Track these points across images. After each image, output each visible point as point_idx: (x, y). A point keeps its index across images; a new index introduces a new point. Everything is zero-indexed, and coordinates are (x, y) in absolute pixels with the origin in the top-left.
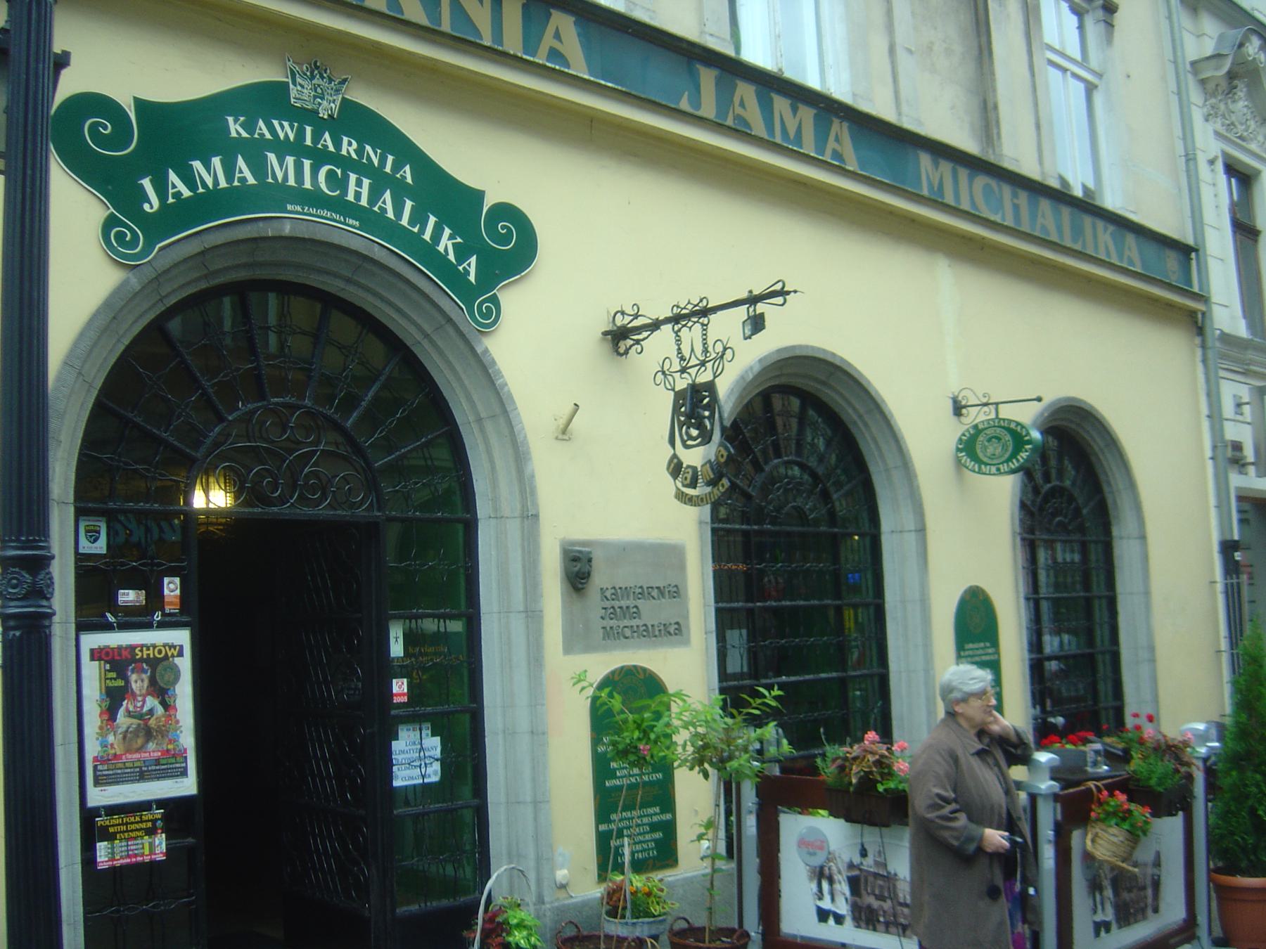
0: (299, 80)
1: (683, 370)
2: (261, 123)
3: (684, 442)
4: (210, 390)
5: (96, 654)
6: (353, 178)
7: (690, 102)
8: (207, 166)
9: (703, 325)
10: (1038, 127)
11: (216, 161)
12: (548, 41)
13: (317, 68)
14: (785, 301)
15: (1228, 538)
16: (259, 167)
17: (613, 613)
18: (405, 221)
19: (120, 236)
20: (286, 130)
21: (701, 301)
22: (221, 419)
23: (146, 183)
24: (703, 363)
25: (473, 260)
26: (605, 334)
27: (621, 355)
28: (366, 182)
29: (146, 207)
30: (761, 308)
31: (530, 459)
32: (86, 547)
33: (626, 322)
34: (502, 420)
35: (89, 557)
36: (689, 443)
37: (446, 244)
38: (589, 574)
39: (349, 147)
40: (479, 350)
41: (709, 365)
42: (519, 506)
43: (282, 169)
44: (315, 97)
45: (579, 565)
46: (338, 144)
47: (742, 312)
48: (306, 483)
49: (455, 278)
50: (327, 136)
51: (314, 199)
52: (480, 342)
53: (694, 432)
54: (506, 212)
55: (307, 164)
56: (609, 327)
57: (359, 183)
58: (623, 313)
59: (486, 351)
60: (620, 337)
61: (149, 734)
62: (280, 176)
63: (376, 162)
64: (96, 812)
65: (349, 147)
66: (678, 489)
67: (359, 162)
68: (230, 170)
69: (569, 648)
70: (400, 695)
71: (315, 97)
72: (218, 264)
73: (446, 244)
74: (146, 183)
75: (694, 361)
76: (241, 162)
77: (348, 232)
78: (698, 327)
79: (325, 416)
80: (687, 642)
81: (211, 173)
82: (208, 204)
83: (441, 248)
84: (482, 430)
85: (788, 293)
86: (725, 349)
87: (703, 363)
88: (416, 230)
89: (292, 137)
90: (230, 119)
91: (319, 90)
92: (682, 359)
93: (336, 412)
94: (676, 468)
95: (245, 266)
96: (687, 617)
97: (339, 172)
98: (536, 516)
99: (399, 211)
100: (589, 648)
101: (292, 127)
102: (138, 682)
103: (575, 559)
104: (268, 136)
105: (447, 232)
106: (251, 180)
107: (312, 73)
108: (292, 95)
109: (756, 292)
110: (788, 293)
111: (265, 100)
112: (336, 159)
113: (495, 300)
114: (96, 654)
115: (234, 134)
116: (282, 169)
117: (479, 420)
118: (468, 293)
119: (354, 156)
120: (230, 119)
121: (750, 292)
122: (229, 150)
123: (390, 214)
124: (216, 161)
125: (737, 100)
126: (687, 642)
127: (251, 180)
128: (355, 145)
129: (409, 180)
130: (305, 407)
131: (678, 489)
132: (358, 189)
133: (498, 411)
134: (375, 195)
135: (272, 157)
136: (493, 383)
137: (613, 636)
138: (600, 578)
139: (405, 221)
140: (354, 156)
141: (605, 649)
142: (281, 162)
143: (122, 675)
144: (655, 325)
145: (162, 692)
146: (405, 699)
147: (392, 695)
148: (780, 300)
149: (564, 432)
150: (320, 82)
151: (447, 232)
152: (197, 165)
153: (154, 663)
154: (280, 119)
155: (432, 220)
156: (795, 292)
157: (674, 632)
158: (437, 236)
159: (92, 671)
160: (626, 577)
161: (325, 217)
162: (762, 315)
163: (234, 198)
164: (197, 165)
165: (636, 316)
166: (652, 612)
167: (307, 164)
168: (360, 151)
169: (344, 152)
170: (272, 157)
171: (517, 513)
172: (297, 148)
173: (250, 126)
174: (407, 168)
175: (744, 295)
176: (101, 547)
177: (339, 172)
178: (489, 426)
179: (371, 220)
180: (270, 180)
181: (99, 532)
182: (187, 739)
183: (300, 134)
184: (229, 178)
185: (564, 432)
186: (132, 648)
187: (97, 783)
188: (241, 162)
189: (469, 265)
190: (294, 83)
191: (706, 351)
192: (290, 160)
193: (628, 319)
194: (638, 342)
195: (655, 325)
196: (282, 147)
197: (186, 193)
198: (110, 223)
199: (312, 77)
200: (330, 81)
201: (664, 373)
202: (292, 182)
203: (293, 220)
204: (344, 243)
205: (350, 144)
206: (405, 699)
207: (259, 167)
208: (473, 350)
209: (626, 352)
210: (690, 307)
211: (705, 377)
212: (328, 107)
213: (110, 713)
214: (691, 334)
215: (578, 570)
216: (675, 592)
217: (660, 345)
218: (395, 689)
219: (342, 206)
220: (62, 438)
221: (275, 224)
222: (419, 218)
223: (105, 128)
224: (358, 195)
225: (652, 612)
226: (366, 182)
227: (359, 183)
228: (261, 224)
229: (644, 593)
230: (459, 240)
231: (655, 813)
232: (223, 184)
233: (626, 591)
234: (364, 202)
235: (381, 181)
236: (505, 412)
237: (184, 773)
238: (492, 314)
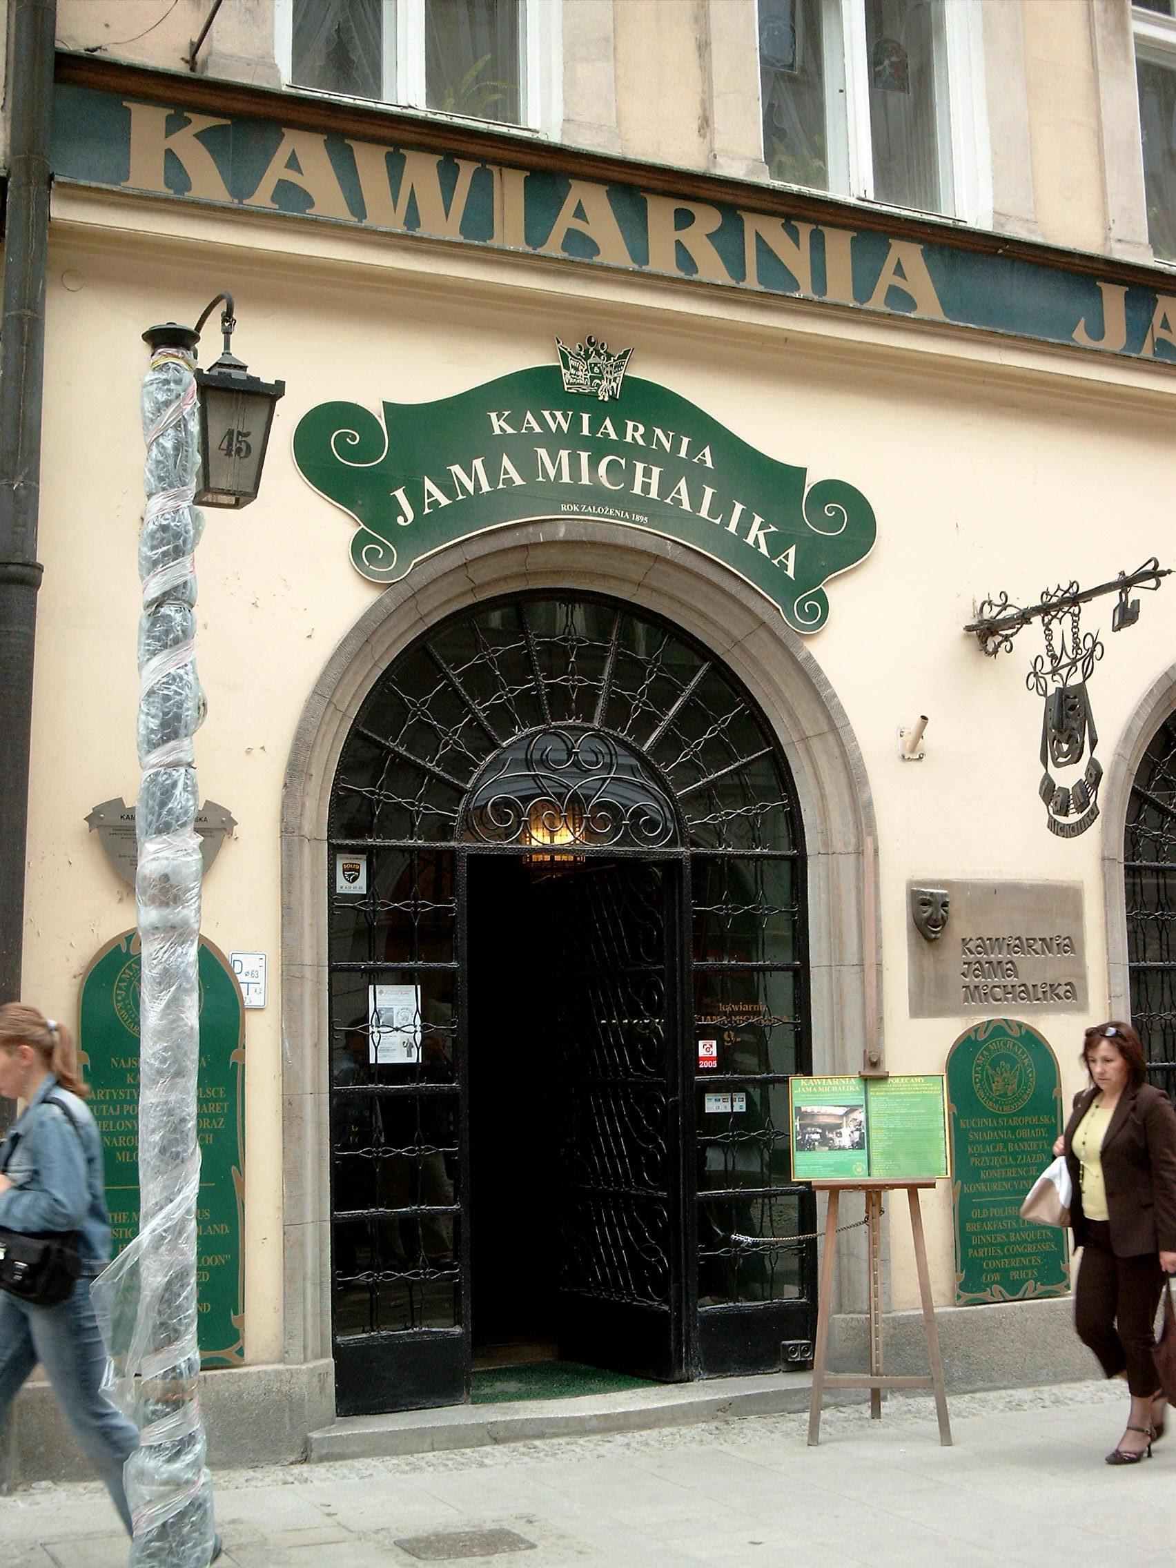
0: (571, 362)
1: (1054, 672)
2: (529, 416)
3: (1054, 760)
4: (482, 715)
6: (640, 467)
7: (1088, 331)
8: (468, 470)
9: (1073, 615)
11: (478, 463)
12: (887, 278)
13: (592, 344)
14: (1158, 584)
16: (527, 465)
17: (978, 968)
18: (704, 513)
20: (558, 420)
21: (1071, 586)
22: (495, 746)
23: (400, 494)
24: (1074, 663)
25: (792, 551)
26: (969, 629)
27: (988, 654)
28: (656, 471)
29: (400, 520)
30: (1134, 593)
31: (867, 783)
32: (343, 886)
33: (994, 614)
34: (831, 738)
35: (347, 897)
36: (1061, 760)
38: (944, 921)
39: (634, 432)
40: (800, 657)
41: (1079, 664)
42: (853, 841)
43: (555, 466)
44: (592, 378)
45: (930, 910)
46: (621, 431)
47: (1113, 598)
48: (593, 818)
49: (773, 576)
50: (608, 422)
51: (594, 495)
52: (802, 647)
53: (1065, 747)
54: (835, 490)
55: (584, 456)
56: (974, 622)
57: (647, 473)
58: (990, 603)
59: (810, 657)
60: (989, 632)
62: (552, 473)
63: (668, 446)
66: (1051, 817)
67: (646, 449)
68: (493, 471)
69: (918, 1010)
70: (705, 1059)
71: (592, 378)
72: (484, 573)
73: (756, 534)
74: (400, 494)
75: (1065, 660)
76: (506, 462)
77: (634, 529)
78: (1068, 617)
79: (616, 739)
81: (473, 477)
82: (467, 509)
83: (750, 540)
84: (808, 751)
85: (1163, 574)
86: (1095, 644)
87: (1074, 663)
88: (718, 521)
89: (565, 427)
90: (493, 415)
91: (596, 370)
92: (1053, 657)
93: (629, 734)
94: (1048, 790)
95: (516, 576)
96: (1083, 977)
97: (623, 462)
99: (696, 501)
100: (939, 1011)
101: (565, 417)
103: (925, 903)
104: (538, 429)
105: (758, 520)
107: (586, 351)
108: (565, 380)
109: (1129, 574)
110: (1163, 574)
111: (537, 387)
112: (620, 447)
113: (822, 598)
115: (497, 431)
116: (555, 466)
117: (804, 739)
118: (787, 590)
119: (641, 442)
120: (493, 415)
121: (1122, 573)
122: (492, 450)
123: (686, 506)
124: (478, 463)
125: (1157, 320)
127: (518, 481)
128: (642, 429)
129: (709, 464)
130: (593, 729)
131: (1051, 817)
133: (826, 728)
134: (667, 485)
135: (542, 452)
136: (817, 695)
138: (961, 927)
139: (704, 513)
140: (641, 442)
142: (554, 457)
144: (1024, 617)
146: (714, 1064)
147: (697, 1059)
148: (1152, 583)
149: (914, 753)
150: (597, 360)
151: (758, 520)
152: (456, 469)
154: (551, 409)
155: (739, 508)
156: (1169, 572)
157: (1068, 993)
158: (744, 527)
161: (592, 514)
162: (1136, 603)
163: (503, 498)
164: (456, 469)
165: (1005, 606)
166: (1032, 968)
167: (584, 456)
168: (648, 436)
169: (629, 439)
170: (542, 452)
171: (851, 849)
172: (573, 440)
173: (516, 421)
174: (707, 451)
175: (1114, 577)
176: (360, 886)
177: (623, 462)
178: (816, 745)
179: (656, 511)
180: (540, 479)
181: (358, 871)
183: (576, 423)
184: (493, 481)
185: (914, 753)
188: (506, 462)
189: (786, 557)
190: (567, 367)
191: (1076, 647)
192: (564, 454)
193: (996, 610)
194: (1007, 638)
195: (1024, 617)
196: (554, 441)
197: (444, 501)
198: (359, 542)
199: (587, 356)
200: (609, 356)
201: (1036, 674)
202: (566, 479)
203: (568, 521)
204: (629, 543)
205: (636, 429)
206: (714, 1064)
207: (527, 465)
208: (793, 658)
209: (995, 652)
210: (1060, 593)
211: (1076, 679)
212: (607, 389)
214: (1062, 627)
215: (930, 915)
216: (1070, 945)
217: (1030, 639)
218: (702, 1052)
219: (625, 501)
220: (313, 771)
221: (547, 526)
222: (722, 507)
223: (354, 439)
224: (646, 487)
225: (1032, 968)
226: (656, 471)
227: (647, 473)
228: (531, 529)
229: (1023, 945)
230: (773, 529)
232: (486, 488)
233: (997, 942)
234: (654, 494)
235: (672, 469)
236: (834, 729)
238: (819, 611)
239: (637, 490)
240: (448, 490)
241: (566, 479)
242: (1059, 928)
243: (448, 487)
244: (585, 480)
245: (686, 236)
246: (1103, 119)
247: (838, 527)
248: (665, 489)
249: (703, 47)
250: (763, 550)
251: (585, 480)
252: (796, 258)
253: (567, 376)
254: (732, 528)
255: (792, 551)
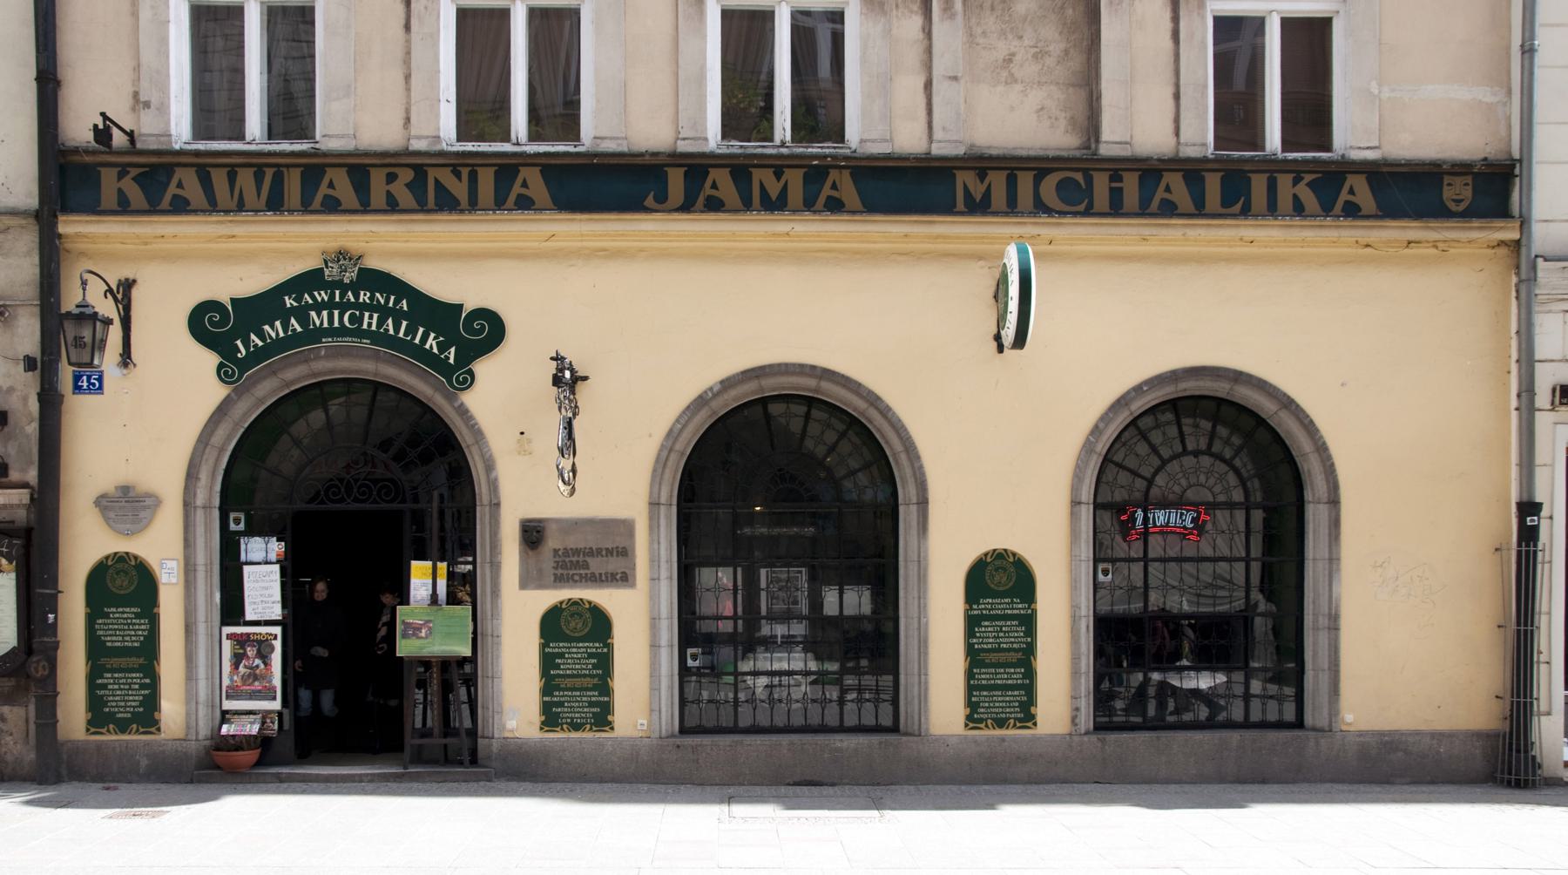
5: (229, 637)
8: (272, 327)
10: (1177, 97)
11: (278, 323)
15: (1525, 499)
16: (304, 320)
18: (401, 335)
19: (226, 373)
20: (322, 296)
23: (239, 342)
25: (453, 350)
26: (585, 378)
28: (375, 316)
37: (431, 343)
39: (364, 297)
43: (319, 319)
46: (357, 296)
55: (336, 313)
61: (256, 678)
64: (227, 712)
65: (364, 297)
68: (285, 326)
69: (525, 584)
73: (431, 343)
74: (239, 342)
76: (293, 321)
80: (633, 585)
96: (634, 569)
98: (498, 505)
99: (397, 330)
100: (541, 586)
102: (251, 652)
106: (299, 329)
113: (471, 374)
114: (229, 637)
123: (391, 332)
124: (278, 323)
126: (633, 585)
127: (299, 329)
132: (370, 321)
134: (380, 323)
135: (313, 314)
137: (560, 580)
138: (552, 542)
139: (401, 335)
141: (555, 588)
143: (243, 647)
145: (264, 656)
152: (267, 327)
153: (260, 642)
154: (319, 290)
155: (421, 330)
157: (624, 579)
159: (227, 646)
160: (574, 542)
164: (267, 327)
167: (336, 313)
170: (313, 314)
172: (330, 305)
182: (277, 681)
183: (332, 296)
184: (285, 331)
186: (248, 635)
187: (228, 697)
188: (293, 321)
192: (325, 313)
196: (318, 308)
207: (304, 320)
212: (350, 276)
213: (236, 666)
215: (532, 534)
216: (625, 552)
224: (370, 325)
229: (591, 553)
231: (595, 647)
232: (282, 334)
233: (577, 552)
234: (374, 328)
235: (384, 313)
237: (274, 698)
238: (469, 381)
239: (365, 326)
240: (262, 338)
241: (326, 325)
242: (620, 542)
243: (262, 336)
244: (336, 324)
245: (393, 188)
246: (681, 62)
247: (486, 331)
248: (379, 325)
249: (408, 77)
250: (435, 350)
251: (336, 324)
252: (460, 189)
253: (327, 272)
254: (417, 341)
255: (453, 350)
